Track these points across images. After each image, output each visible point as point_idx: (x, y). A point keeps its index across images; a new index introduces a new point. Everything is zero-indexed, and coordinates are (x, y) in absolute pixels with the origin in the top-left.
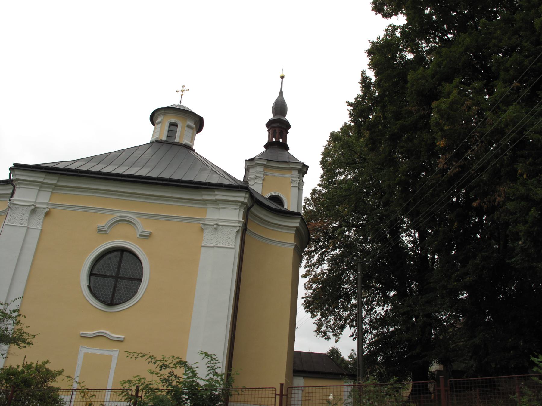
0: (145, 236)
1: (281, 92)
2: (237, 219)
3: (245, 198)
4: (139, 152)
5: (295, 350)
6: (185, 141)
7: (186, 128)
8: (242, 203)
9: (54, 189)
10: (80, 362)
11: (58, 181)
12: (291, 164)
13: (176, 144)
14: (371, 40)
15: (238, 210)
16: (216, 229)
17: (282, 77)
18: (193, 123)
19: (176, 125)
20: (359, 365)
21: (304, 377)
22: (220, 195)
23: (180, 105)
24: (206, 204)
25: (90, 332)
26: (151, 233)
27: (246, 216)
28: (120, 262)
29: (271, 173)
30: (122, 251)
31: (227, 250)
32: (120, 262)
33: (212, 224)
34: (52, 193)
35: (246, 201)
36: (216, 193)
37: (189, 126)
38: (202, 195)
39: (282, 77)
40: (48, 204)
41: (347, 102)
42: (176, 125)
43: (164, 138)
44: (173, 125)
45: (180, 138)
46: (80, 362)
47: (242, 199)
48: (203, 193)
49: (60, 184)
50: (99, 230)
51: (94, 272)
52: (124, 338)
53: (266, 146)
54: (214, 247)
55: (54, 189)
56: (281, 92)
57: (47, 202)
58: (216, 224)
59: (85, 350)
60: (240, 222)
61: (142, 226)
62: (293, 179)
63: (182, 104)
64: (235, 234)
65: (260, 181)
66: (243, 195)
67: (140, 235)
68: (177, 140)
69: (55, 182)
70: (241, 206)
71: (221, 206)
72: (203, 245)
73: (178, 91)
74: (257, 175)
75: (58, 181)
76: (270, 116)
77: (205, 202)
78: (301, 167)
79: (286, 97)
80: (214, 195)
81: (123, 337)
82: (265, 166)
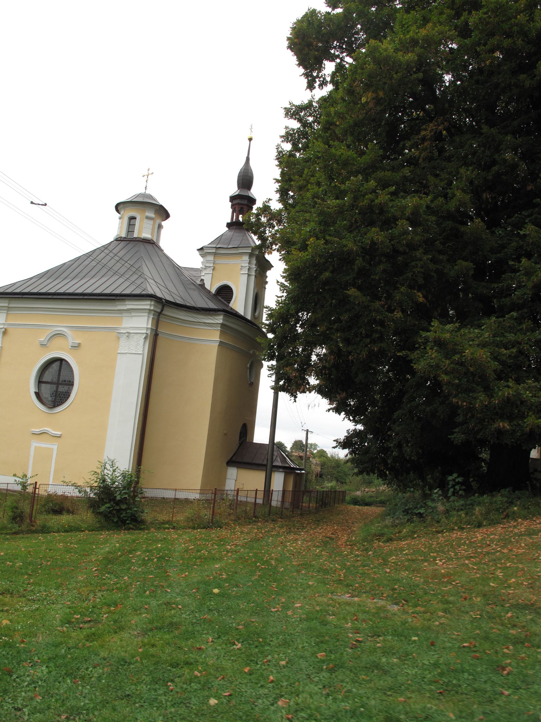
0: (76, 347)
1: (248, 159)
2: (146, 326)
3: (151, 305)
4: (94, 256)
5: (254, 442)
6: (146, 235)
7: (146, 221)
8: (150, 310)
9: (8, 311)
10: (32, 453)
11: (9, 304)
12: (239, 249)
13: (134, 239)
14: (283, 107)
15: (147, 318)
16: (128, 337)
17: (250, 139)
18: (153, 213)
19: (135, 218)
20: (267, 459)
21: (237, 467)
22: (130, 305)
23: (144, 195)
24: (122, 313)
25: (37, 430)
26: (80, 343)
27: (157, 322)
28: (60, 370)
29: (221, 261)
30: (61, 360)
31: (136, 355)
32: (60, 370)
33: (125, 332)
34: (7, 314)
35: (152, 308)
36: (127, 303)
37: (148, 218)
38: (117, 306)
39: (250, 139)
40: (4, 324)
41: (274, 179)
42: (135, 218)
43: (123, 235)
44: (132, 218)
45: (138, 233)
46: (32, 453)
47: (148, 307)
48: (117, 303)
49: (11, 306)
50: (41, 345)
51: (44, 380)
52: (61, 435)
53: (229, 225)
54: (126, 353)
55: (8, 311)
56: (248, 159)
57: (4, 322)
58: (127, 333)
59: (35, 444)
60: (147, 328)
61: (73, 338)
62: (243, 265)
63: (147, 192)
64: (143, 340)
65: (210, 271)
66: (149, 302)
67: (72, 346)
68: (135, 235)
69: (6, 305)
70: (149, 313)
71: (133, 314)
72: (119, 352)
73: (143, 176)
74: (207, 265)
75: (9, 304)
76: (233, 189)
77: (121, 311)
78: (250, 251)
79: (253, 165)
80: (126, 305)
81: (60, 433)
82: (215, 254)
